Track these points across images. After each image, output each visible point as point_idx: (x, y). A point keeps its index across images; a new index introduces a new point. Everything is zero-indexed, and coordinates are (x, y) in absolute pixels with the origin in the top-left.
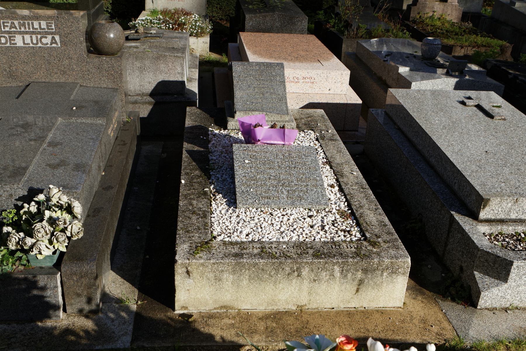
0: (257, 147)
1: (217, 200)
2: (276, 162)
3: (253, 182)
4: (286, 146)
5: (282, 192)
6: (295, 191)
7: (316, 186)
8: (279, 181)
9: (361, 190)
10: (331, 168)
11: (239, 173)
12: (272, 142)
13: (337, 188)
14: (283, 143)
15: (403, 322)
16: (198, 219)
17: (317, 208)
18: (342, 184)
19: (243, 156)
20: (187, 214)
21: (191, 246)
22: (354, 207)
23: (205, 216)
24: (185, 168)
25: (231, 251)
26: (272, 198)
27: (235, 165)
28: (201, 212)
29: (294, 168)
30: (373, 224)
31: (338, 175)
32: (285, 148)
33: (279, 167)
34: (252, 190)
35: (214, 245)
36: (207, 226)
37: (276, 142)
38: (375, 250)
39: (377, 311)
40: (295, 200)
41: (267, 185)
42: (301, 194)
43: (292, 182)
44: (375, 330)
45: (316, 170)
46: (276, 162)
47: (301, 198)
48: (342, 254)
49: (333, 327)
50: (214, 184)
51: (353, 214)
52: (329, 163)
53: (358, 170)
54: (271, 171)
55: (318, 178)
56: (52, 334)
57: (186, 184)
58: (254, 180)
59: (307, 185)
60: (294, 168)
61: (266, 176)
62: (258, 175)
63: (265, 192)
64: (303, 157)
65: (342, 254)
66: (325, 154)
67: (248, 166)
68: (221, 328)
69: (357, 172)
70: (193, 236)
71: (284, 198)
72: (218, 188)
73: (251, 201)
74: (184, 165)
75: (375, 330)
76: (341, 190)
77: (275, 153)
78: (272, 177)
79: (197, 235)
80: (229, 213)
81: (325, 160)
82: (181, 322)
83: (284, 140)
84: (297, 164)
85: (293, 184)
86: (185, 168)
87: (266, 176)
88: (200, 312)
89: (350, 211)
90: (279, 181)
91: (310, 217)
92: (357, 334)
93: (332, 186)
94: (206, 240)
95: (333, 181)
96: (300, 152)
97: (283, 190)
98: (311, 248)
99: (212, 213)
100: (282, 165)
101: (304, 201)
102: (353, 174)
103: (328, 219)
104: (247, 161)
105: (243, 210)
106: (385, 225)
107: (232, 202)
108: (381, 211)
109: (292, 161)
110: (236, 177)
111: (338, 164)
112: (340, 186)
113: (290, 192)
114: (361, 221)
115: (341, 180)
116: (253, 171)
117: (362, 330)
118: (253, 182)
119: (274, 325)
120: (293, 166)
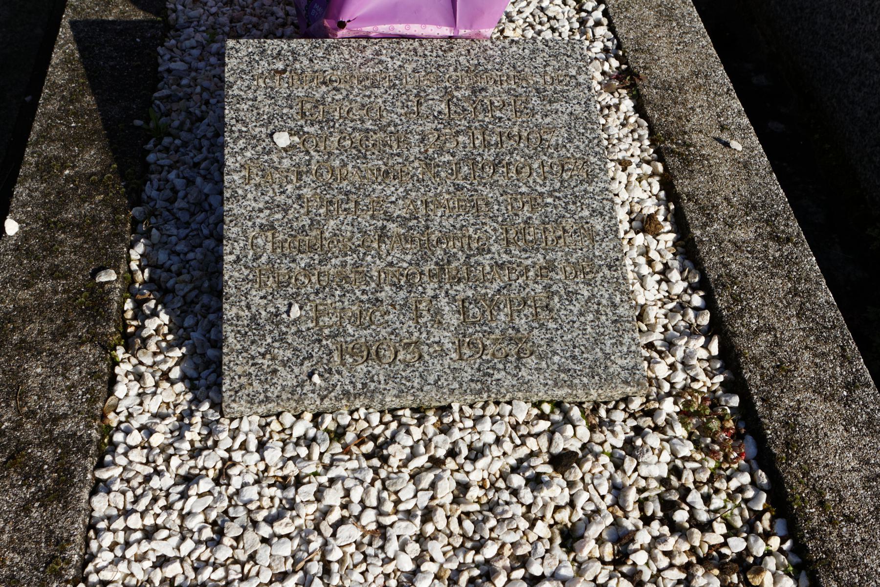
0: (335, 57)
1: (145, 341)
2: (414, 139)
3: (304, 260)
4: (461, 46)
5: (437, 316)
6: (494, 305)
7: (586, 270)
8: (426, 249)
9: (773, 250)
10: (639, 109)
11: (245, 202)
12: (400, 28)
13: (668, 238)
14: (446, 31)
16: (26, 508)
18: (692, 215)
19: (266, 109)
22: (752, 376)
23: (60, 491)
24: (44, 136)
26: (389, 354)
27: (230, 162)
29: (495, 166)
31: (670, 153)
32: (458, 56)
33: (427, 162)
34: (295, 312)
37: (415, 29)
40: (496, 353)
41: (366, 277)
42: (521, 322)
43: (481, 251)
45: (591, 178)
46: (414, 139)
47: (520, 347)
50: (147, 235)
52: (628, 78)
53: (746, 121)
54: (393, 190)
55: (598, 225)
56: (167, 37)
57: (24, 236)
58: (312, 248)
59: (550, 267)
60: (495, 166)
61: (364, 220)
62: (329, 215)
63: (358, 320)
64: (535, 101)
66: (611, 28)
67: (286, 163)
69: (745, 143)
71: (443, 353)
72: (162, 256)
73: (291, 382)
74: (48, 105)
76: (687, 249)
77: (411, 83)
78: (391, 226)
81: (615, 63)
83: (453, 24)
84: (509, 144)
85: (486, 260)
86: (44, 136)
87: (364, 220)
89: (735, 401)
90: (426, 249)
93: (646, 225)
95: (647, 196)
96: (520, 77)
97: (443, 301)
99: (105, 450)
100: (441, 151)
101: (532, 361)
102: (733, 147)
104: (283, 139)
105: (250, 425)
107: (205, 377)
109: (484, 129)
110: (232, 231)
111: (666, 87)
112: (680, 224)
113: (474, 310)
114: (791, 472)
115: (683, 186)
116: (307, 192)
118: (304, 260)
120: (489, 155)
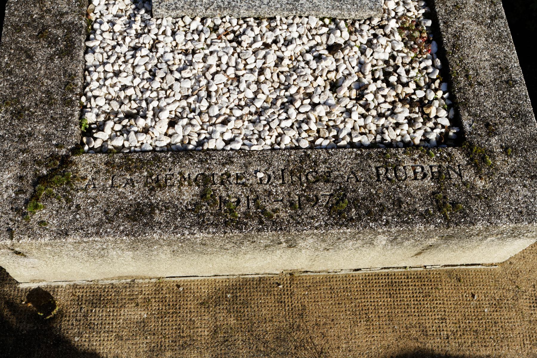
15: (497, 305)
17: (353, 17)
20: (25, 38)
21: (21, 178)
25: (122, 196)
28: (59, 32)
30: (482, 78)
35: (82, 173)
36: (71, 90)
38: (480, 184)
39: (449, 274)
44: (439, 330)
48: (400, 202)
49: (355, 323)
51: (435, 33)
65: (400, 202)
68: (117, 336)
70: (30, 135)
75: (439, 330)
79: (41, 127)
80: (133, 32)
82: (32, 317)
88: (75, 286)
89: (429, 23)
91: (333, 49)
92: (401, 344)
94: (63, 152)
98: (327, 179)
99: (90, 32)
103: (376, 56)
105: (167, 23)
106: (510, 83)
108: (503, 23)
114: (453, 60)
117: (413, 332)
119: (232, 321)
